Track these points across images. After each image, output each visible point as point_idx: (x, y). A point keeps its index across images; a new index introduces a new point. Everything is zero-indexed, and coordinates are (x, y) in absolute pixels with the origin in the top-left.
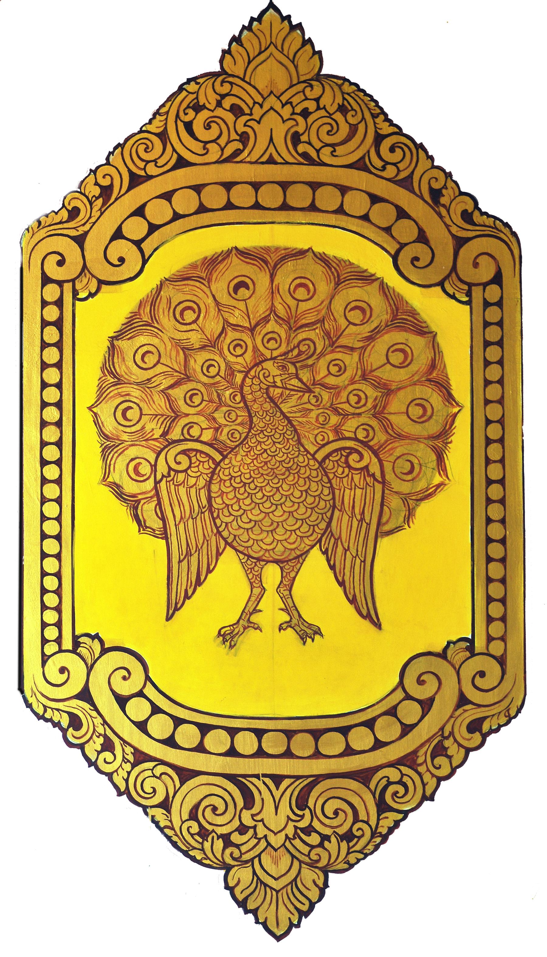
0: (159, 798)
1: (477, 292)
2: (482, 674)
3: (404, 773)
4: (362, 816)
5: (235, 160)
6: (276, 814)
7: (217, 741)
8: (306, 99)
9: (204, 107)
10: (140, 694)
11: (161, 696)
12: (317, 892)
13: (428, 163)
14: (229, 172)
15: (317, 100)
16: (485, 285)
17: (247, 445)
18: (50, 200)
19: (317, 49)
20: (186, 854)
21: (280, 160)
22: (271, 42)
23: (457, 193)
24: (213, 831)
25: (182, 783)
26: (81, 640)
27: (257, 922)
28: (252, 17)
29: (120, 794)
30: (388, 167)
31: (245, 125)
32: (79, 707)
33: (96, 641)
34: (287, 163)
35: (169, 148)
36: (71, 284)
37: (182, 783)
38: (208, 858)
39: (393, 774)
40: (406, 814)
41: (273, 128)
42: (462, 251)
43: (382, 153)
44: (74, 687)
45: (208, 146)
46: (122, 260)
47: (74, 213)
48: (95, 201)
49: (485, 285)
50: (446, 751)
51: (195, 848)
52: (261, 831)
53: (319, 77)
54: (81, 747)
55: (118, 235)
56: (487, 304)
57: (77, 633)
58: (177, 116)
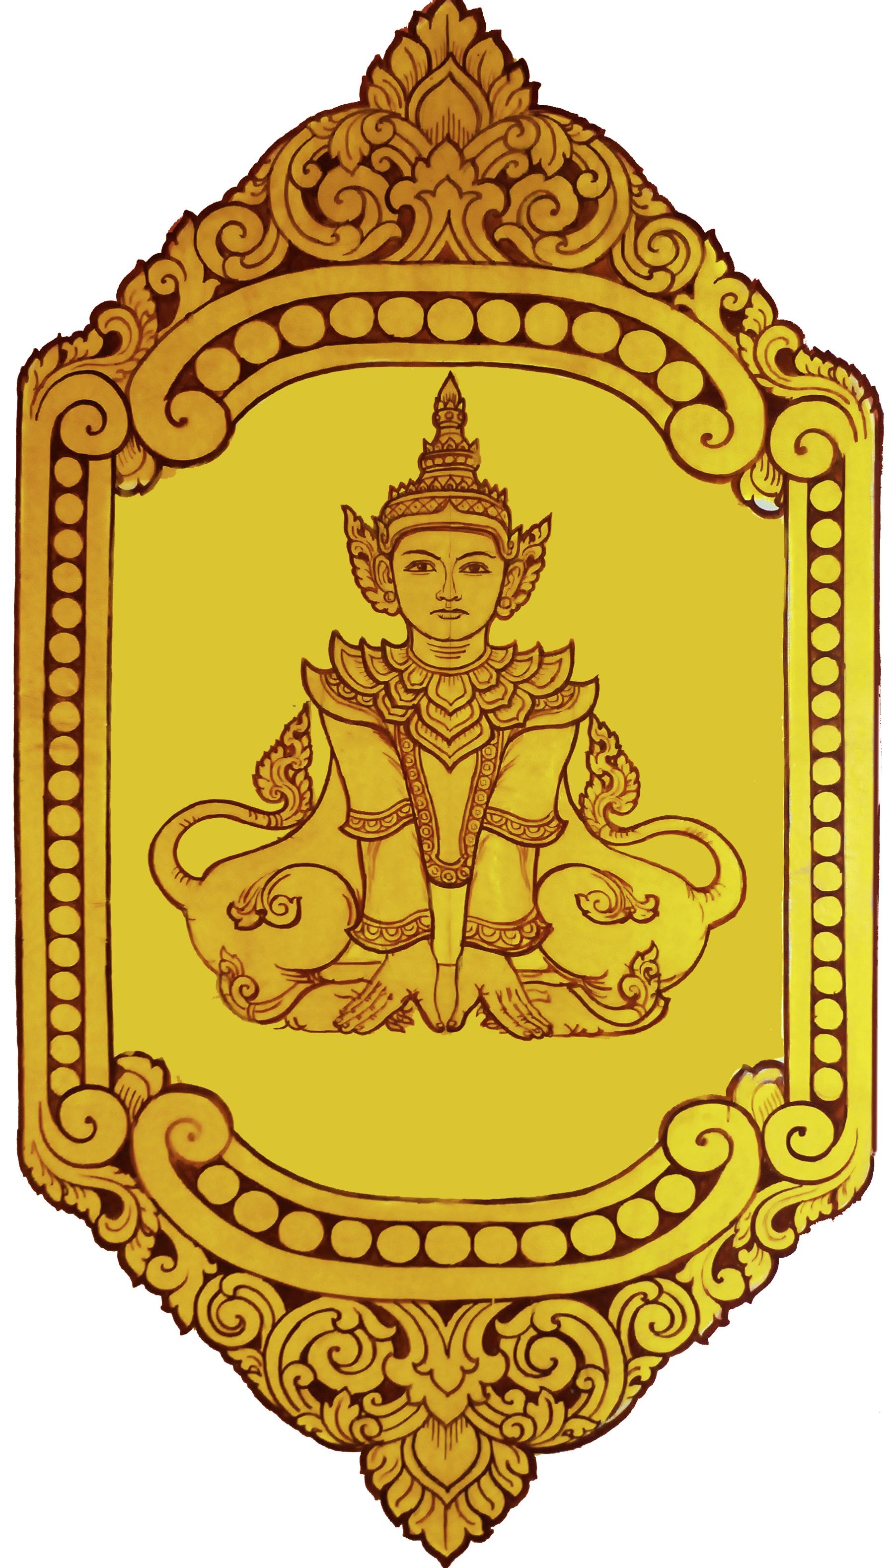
4: (593, 1355)
5: (508, 1304)
8: (512, 150)
9: (559, 1396)
10: (219, 1161)
12: (518, 1484)
13: (722, 267)
14: (517, 1283)
16: (812, 482)
17: (130, 460)
18: (821, 1245)
23: (769, 321)
27: (478, 14)
28: (415, 12)
29: (184, 1330)
32: (115, 1181)
35: (272, 231)
36: (108, 462)
37: (609, 254)
38: (563, 127)
40: (665, 1358)
44: (108, 1144)
45: (552, 1327)
46: (701, 1141)
48: (147, 322)
49: (812, 482)
54: (119, 1248)
56: (814, 516)
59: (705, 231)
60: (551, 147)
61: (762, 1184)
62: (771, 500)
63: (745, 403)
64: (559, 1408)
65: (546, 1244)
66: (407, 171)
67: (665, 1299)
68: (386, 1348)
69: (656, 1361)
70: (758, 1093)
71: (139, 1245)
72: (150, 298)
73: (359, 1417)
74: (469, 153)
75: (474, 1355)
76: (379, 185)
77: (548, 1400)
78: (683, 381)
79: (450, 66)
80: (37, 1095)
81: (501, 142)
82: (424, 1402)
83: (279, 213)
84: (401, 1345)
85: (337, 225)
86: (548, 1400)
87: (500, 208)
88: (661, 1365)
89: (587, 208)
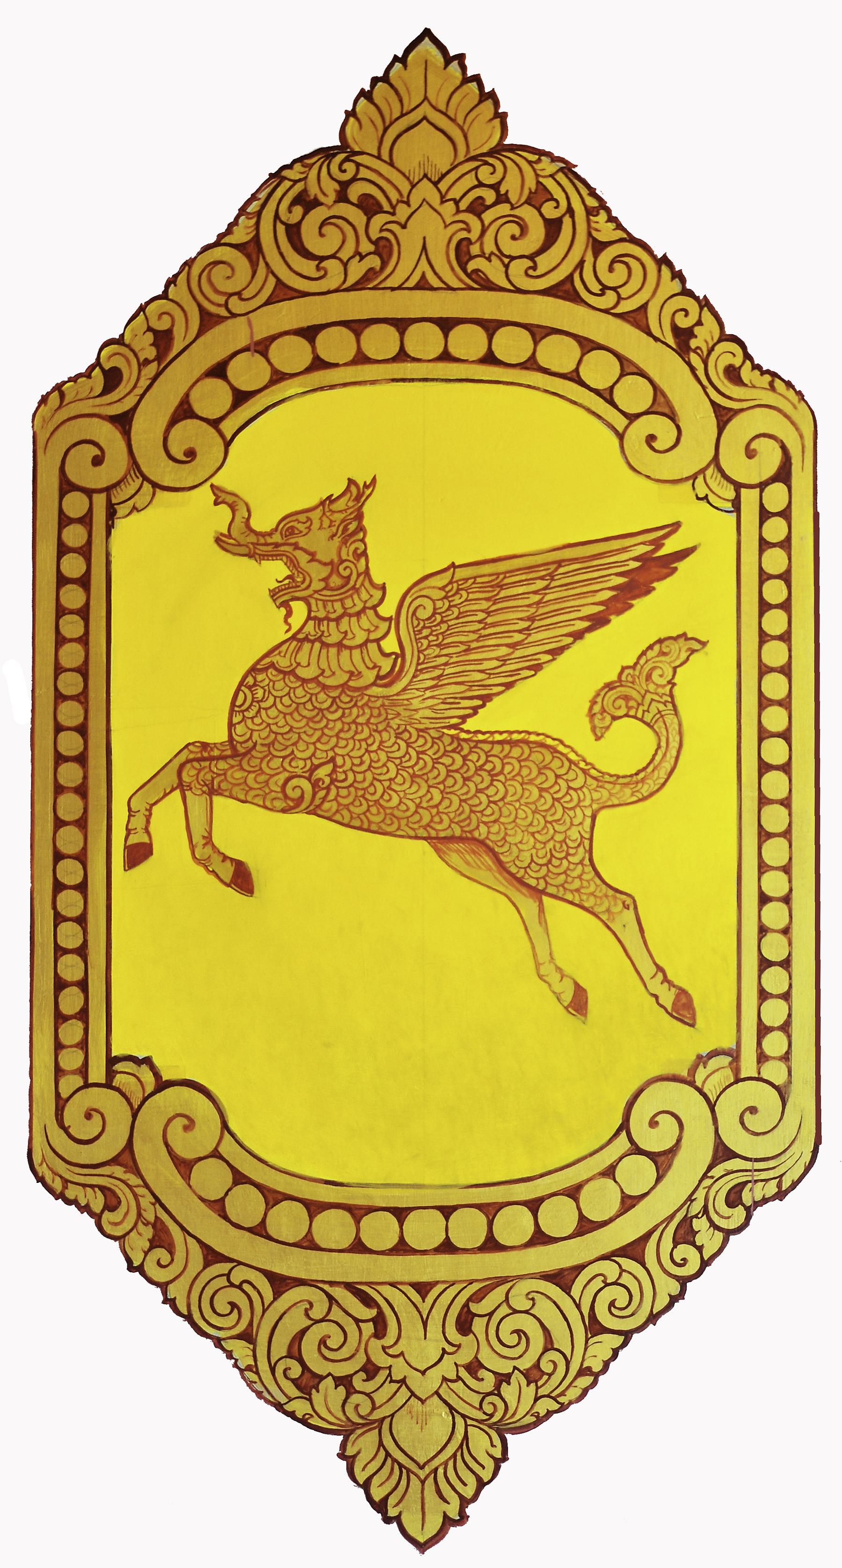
1: (749, 497)
2: (97, 461)
6: (424, 238)
8: (481, 185)
10: (216, 1154)
12: (490, 1465)
13: (676, 286)
15: (495, 187)
20: (279, 1407)
30: (608, 292)
35: (262, 270)
39: (610, 1269)
40: (627, 1336)
41: (420, 1345)
42: (122, 1143)
44: (740, 429)
45: (324, 264)
47: (113, 378)
49: (762, 486)
50: (694, 1237)
53: (501, 149)
54: (725, 337)
56: (764, 515)
58: (277, 217)
59: (659, 257)
64: (313, 190)
66: (463, 1373)
68: (368, 1329)
69: (226, 240)
70: (714, 1076)
71: (706, 342)
72: (151, 340)
73: (499, 183)
74: (404, 1393)
76: (486, 1356)
77: (325, 194)
79: (425, 109)
80: (800, 477)
82: (403, 1381)
85: (322, 259)
86: (325, 194)
87: (373, 1339)
88: (625, 1344)
89: (553, 228)
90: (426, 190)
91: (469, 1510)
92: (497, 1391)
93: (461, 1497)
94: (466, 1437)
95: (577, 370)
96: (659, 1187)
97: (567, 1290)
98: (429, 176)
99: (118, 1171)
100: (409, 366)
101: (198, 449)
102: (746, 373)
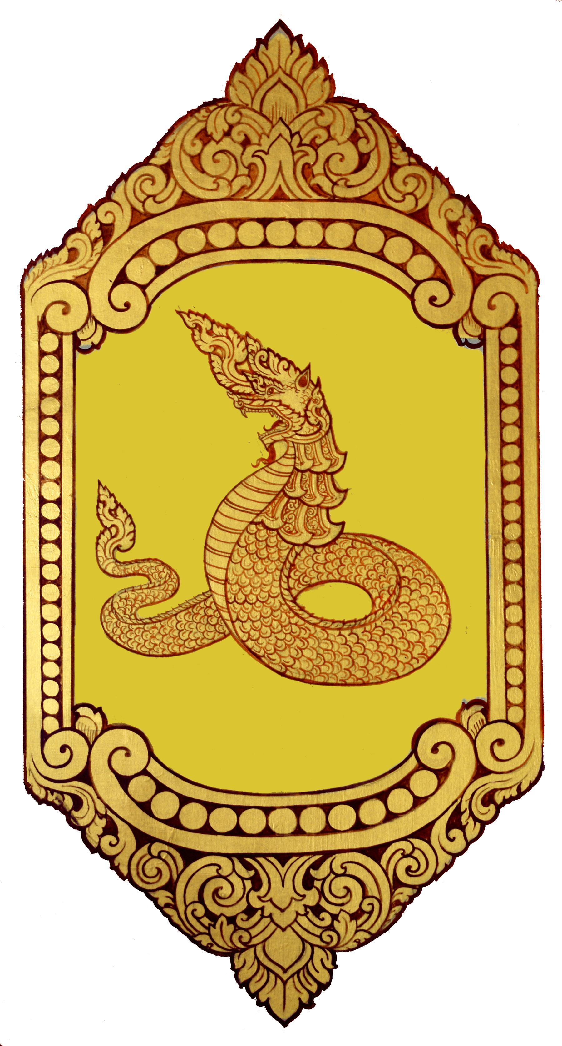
0: (165, 880)
2: (501, 742)
3: (415, 846)
4: (372, 890)
5: (321, 856)
7: (223, 820)
8: (247, 930)
10: (144, 772)
11: (71, 560)
19: (295, 34)
20: (192, 938)
21: (291, 197)
22: (280, 67)
24: (222, 914)
25: (186, 865)
26: (81, 711)
31: (253, 156)
33: (98, 714)
34: (299, 200)
35: (172, 182)
40: (418, 889)
41: (282, 888)
43: (396, 183)
51: (200, 933)
52: (269, 909)
55: (122, 278)
57: (75, 704)
60: (223, 934)
61: (476, 777)
62: (477, 339)
63: (103, 778)
65: (343, 817)
67: (142, 197)
68: (249, 884)
73: (235, 931)
75: (302, 894)
78: (141, 788)
79: (285, 977)
81: (253, 936)
83: (176, 171)
84: (257, 883)
88: (417, 894)
90: (281, 128)
91: (316, 1000)
92: (231, 127)
93: (309, 991)
94: (253, 99)
95: (382, 250)
96: (439, 791)
97: (184, 193)
98: (284, 118)
99: (80, 784)
100: (292, 804)
101: (130, 302)
102: (495, 252)
